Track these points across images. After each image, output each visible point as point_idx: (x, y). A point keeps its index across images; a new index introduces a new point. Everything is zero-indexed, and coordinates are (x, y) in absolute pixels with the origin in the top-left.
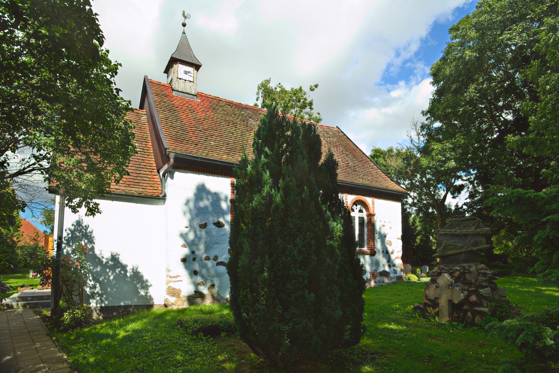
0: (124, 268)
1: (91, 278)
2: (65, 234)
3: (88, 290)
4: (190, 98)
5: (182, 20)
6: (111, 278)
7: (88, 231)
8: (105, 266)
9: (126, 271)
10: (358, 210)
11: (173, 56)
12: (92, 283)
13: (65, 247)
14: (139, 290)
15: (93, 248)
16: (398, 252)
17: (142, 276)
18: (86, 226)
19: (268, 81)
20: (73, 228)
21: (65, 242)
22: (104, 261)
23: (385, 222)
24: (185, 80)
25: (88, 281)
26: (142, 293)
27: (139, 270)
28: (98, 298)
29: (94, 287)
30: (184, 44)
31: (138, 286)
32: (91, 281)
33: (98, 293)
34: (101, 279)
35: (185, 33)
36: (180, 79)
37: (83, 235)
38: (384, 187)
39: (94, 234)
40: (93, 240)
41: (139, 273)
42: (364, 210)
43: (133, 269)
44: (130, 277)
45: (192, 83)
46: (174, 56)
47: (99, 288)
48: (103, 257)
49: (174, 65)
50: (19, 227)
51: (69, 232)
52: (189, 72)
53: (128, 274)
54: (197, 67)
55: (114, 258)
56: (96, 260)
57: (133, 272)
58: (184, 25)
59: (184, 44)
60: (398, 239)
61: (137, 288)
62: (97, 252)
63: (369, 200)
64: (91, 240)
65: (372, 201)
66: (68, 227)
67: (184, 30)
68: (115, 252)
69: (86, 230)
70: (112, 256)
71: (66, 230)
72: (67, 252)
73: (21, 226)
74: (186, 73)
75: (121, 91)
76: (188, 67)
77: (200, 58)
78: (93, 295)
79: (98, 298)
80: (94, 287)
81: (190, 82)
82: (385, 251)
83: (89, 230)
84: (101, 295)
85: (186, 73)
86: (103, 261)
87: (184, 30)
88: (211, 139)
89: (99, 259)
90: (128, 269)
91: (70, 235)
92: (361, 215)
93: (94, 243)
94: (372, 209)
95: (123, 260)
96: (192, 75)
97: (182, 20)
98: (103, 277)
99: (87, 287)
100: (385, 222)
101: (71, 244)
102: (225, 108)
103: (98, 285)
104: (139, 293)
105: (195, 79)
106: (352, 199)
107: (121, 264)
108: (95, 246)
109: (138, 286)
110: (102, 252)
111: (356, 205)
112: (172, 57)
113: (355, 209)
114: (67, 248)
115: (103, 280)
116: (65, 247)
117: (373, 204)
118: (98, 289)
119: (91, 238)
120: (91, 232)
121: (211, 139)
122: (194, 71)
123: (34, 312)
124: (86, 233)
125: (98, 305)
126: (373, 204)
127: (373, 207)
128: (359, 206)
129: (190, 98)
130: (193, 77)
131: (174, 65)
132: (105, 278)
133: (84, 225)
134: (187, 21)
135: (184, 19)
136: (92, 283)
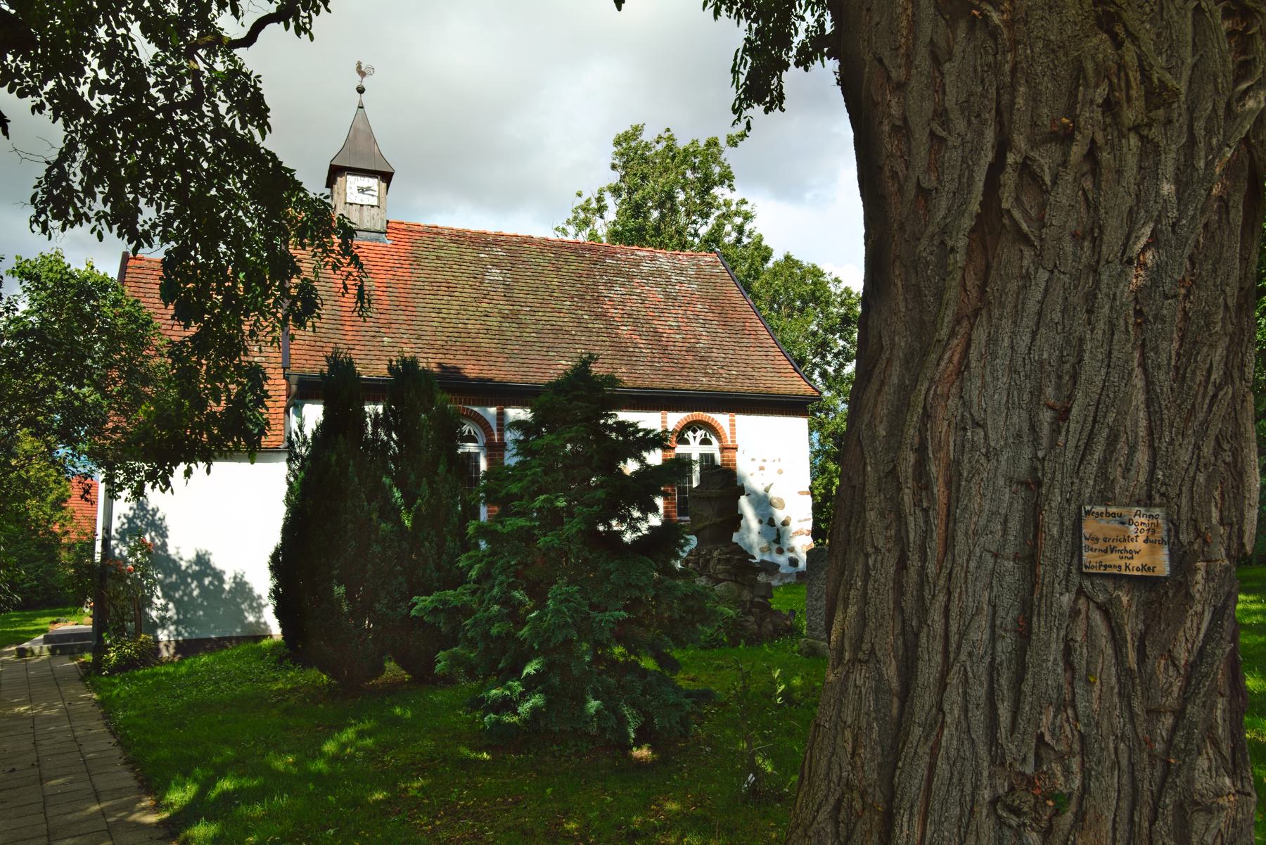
0: (218, 576)
1: (159, 593)
2: (116, 524)
3: (154, 614)
4: (371, 240)
5: (356, 80)
6: (196, 593)
7: (157, 518)
8: (183, 575)
9: (222, 581)
10: (698, 440)
11: (333, 163)
12: (163, 601)
13: (117, 545)
14: (246, 614)
15: (164, 545)
16: (800, 521)
17: (251, 590)
18: (153, 510)
19: (637, 130)
20: (131, 513)
21: (118, 536)
22: (184, 565)
23: (764, 461)
24: (362, 205)
25: (155, 599)
26: (251, 618)
27: (246, 579)
28: (172, 628)
29: (165, 609)
30: (360, 133)
31: (243, 606)
32: (158, 598)
33: (170, 618)
34: (177, 595)
35: (362, 107)
36: (351, 204)
37: (147, 525)
38: (762, 388)
39: (167, 522)
40: (164, 532)
41: (246, 583)
42: (713, 440)
43: (235, 577)
44: (230, 591)
45: (376, 208)
46: (336, 163)
47: (174, 611)
48: (181, 559)
49: (339, 179)
50: (65, 501)
51: (125, 521)
52: (368, 189)
53: (227, 587)
54: (386, 177)
55: (202, 560)
56: (169, 565)
57: (234, 582)
58: (361, 90)
59: (360, 133)
60: (801, 493)
61: (242, 611)
62: (171, 550)
63: (721, 420)
64: (162, 532)
65: (731, 420)
66: (123, 512)
67: (361, 102)
68: (203, 548)
69: (154, 515)
70: (198, 556)
71: (119, 518)
72: (120, 554)
73: (70, 496)
74: (362, 190)
75: (312, 38)
76: (366, 179)
77: (394, 161)
78: (163, 622)
79: (172, 628)
80: (165, 609)
81: (372, 206)
82: (766, 520)
83: (159, 515)
84: (177, 623)
85: (362, 190)
86: (180, 566)
87: (361, 102)
88: (387, 330)
89: (174, 561)
90: (226, 577)
91: (126, 526)
92: (706, 449)
93: (167, 537)
94: (728, 435)
95: (217, 562)
96: (376, 194)
97: (356, 80)
98: (181, 593)
99: (152, 609)
100: (764, 461)
101: (128, 539)
102: (442, 253)
103: (171, 606)
104: (246, 618)
105: (382, 200)
106: (678, 420)
107: (214, 569)
108: (167, 540)
109: (243, 606)
110: (180, 550)
111: (694, 431)
112: (331, 165)
113: (691, 440)
114: (120, 546)
115: (182, 597)
116: (117, 545)
117: (732, 425)
118: (172, 613)
119: (161, 528)
120: (162, 520)
121: (387, 330)
122: (379, 185)
123: (264, 127)
124: (153, 520)
125: (172, 639)
126: (732, 425)
127: (733, 433)
128: (700, 434)
129: (371, 240)
130: (379, 197)
131: (339, 179)
132: (185, 594)
133: (150, 508)
134: (366, 83)
135: (359, 78)
136: (163, 601)
